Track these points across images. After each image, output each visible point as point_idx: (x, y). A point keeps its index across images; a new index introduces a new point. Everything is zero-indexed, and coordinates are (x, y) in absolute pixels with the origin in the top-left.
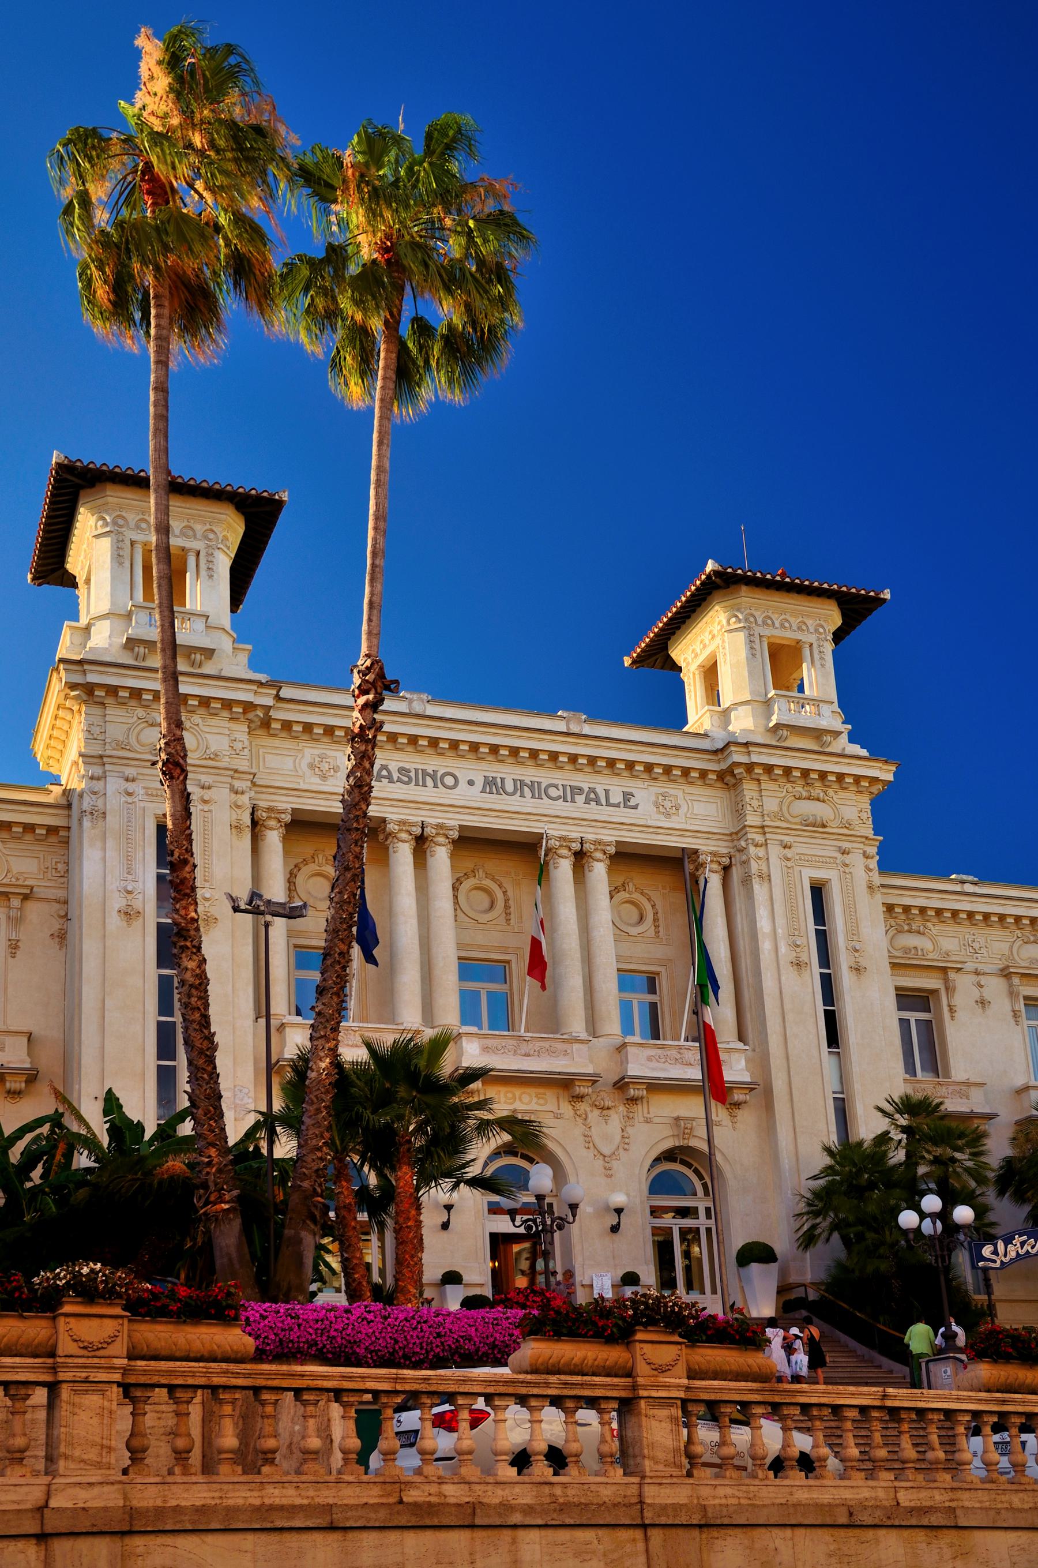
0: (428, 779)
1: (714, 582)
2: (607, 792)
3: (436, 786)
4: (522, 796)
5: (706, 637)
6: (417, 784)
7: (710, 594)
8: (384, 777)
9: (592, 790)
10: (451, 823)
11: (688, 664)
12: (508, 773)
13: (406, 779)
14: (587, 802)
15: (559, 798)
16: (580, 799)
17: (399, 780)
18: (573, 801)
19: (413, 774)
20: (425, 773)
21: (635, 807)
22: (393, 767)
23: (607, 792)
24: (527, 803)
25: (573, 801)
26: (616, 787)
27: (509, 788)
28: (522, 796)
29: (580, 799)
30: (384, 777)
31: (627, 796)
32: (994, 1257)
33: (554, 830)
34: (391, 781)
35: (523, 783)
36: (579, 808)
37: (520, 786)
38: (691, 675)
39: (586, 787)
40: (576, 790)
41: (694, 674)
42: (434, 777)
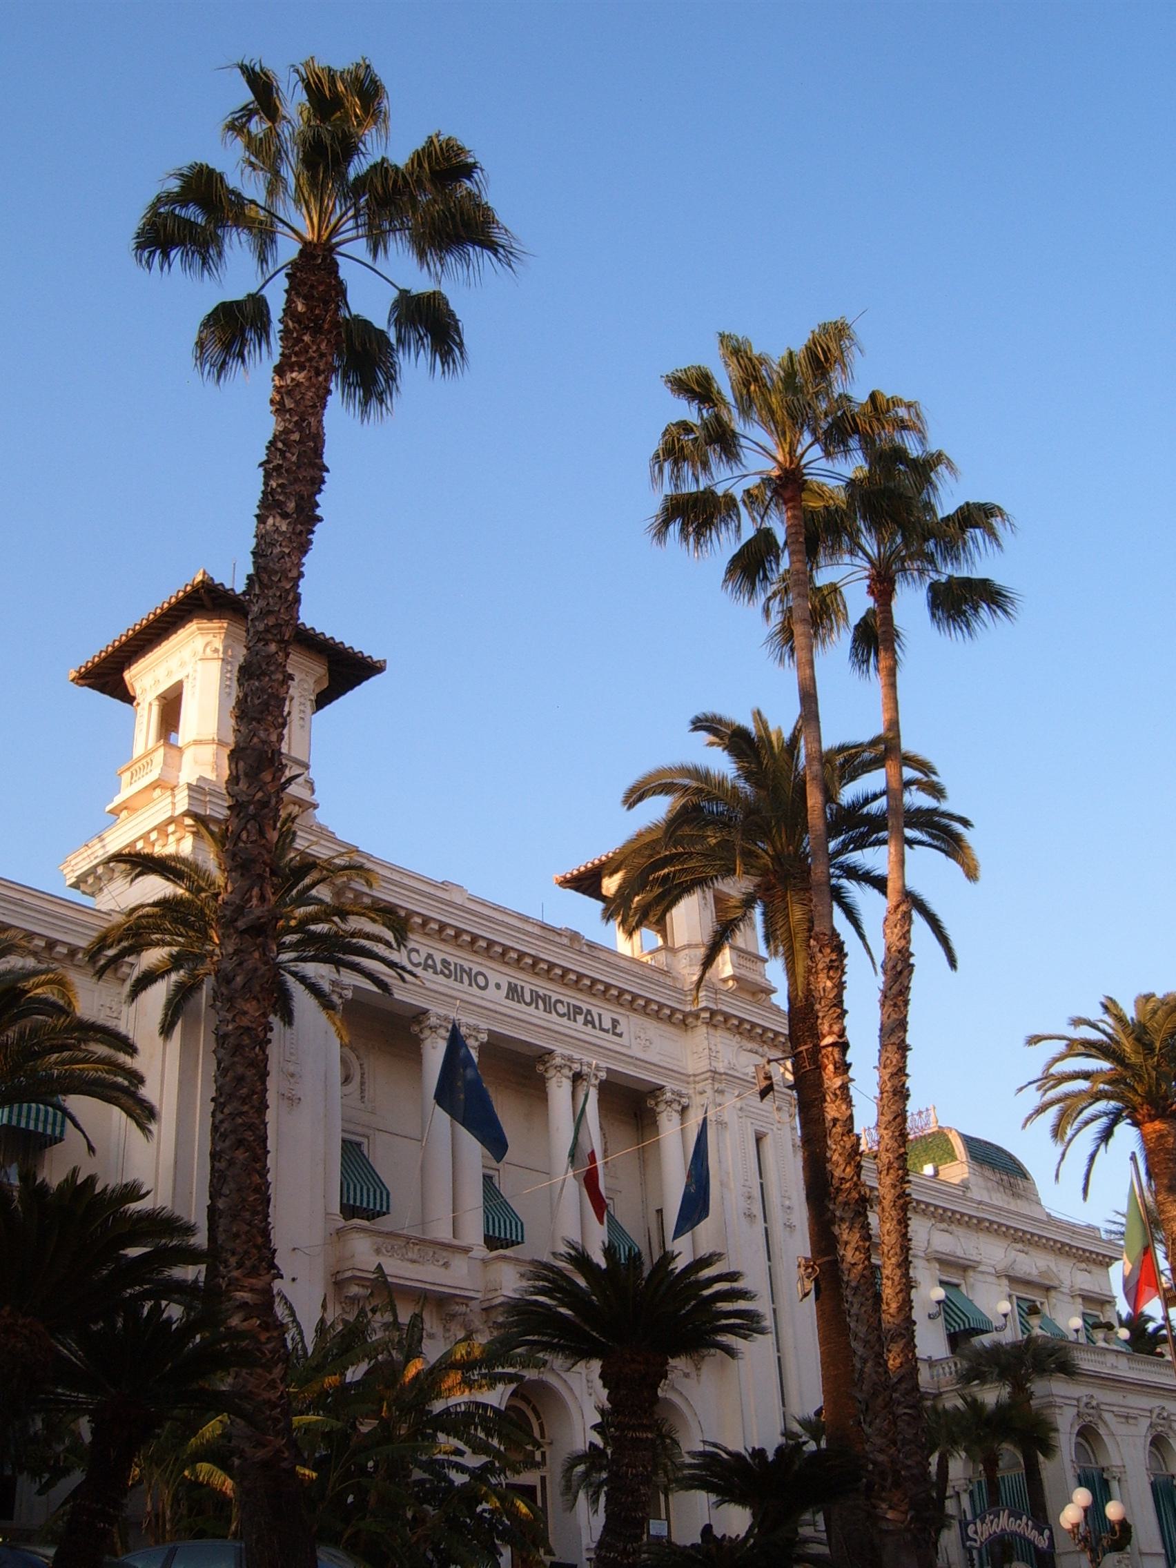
0: (465, 976)
1: (200, 599)
2: (600, 1015)
3: (470, 985)
4: (537, 1007)
5: (173, 663)
6: (456, 980)
7: (190, 612)
8: (430, 966)
9: (589, 1012)
10: (483, 1026)
11: (144, 691)
12: (529, 983)
13: (447, 972)
14: (586, 1023)
15: (564, 1015)
16: (580, 1018)
17: (442, 972)
18: (575, 1020)
19: (452, 968)
20: (463, 970)
21: (620, 1035)
22: (438, 957)
23: (600, 1015)
24: (536, 1014)
25: (575, 1020)
26: (606, 1013)
27: (528, 999)
28: (537, 1007)
29: (580, 1018)
30: (430, 966)
31: (615, 1023)
32: (974, 1536)
33: (437, 1010)
34: (435, 973)
35: (538, 996)
36: (577, 1027)
37: (536, 997)
38: (146, 706)
39: (585, 1007)
40: (578, 1010)
41: (150, 704)
42: (469, 975)
